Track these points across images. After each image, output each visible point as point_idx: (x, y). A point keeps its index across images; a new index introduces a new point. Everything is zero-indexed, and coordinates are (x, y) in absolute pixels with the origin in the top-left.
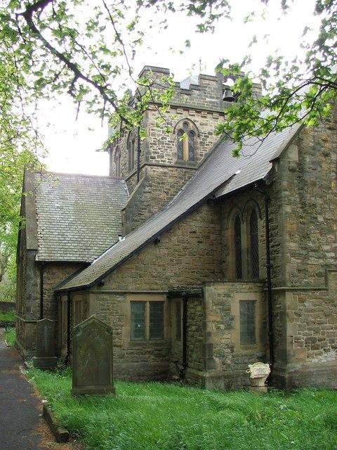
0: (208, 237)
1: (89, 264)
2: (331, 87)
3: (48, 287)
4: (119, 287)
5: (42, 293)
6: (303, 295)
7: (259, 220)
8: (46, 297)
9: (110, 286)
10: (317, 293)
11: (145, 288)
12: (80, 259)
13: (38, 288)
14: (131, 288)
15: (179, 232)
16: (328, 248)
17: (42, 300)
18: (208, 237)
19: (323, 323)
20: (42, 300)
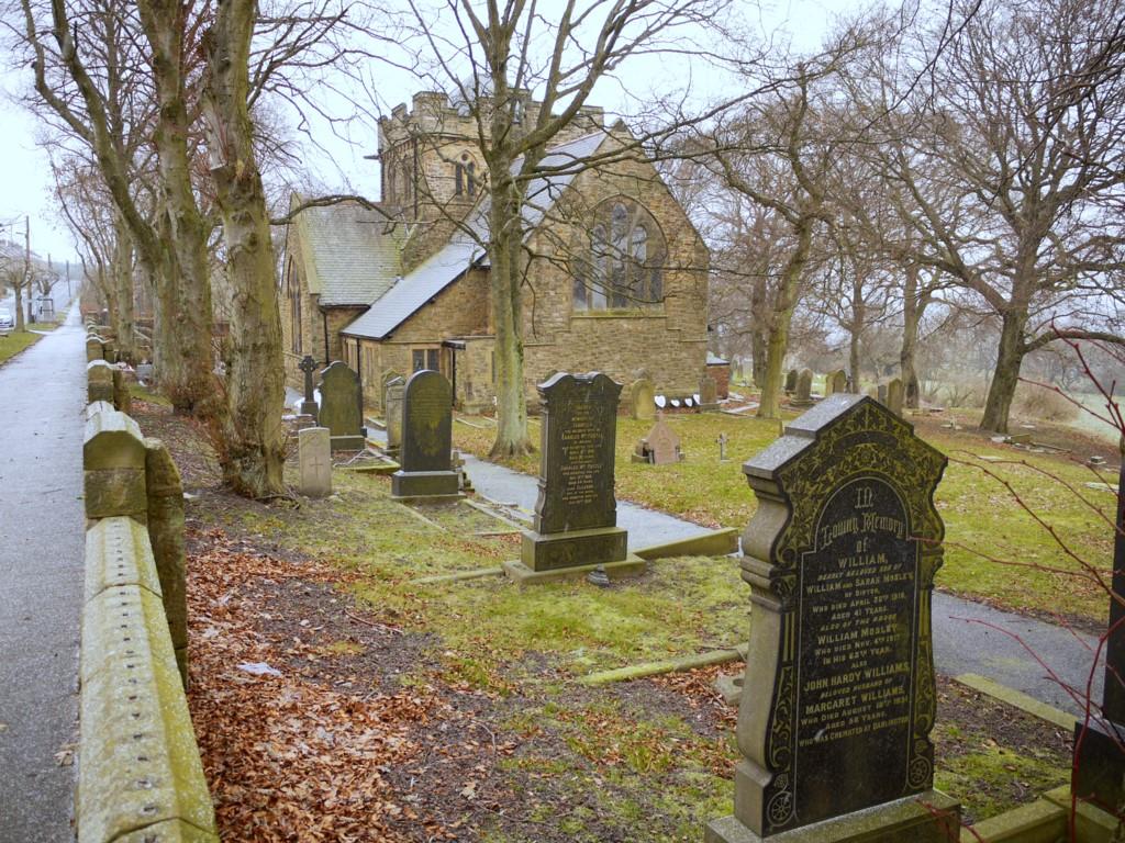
0: (475, 297)
1: (369, 307)
2: (459, 180)
3: (333, 329)
4: (403, 339)
5: (326, 335)
6: (535, 349)
7: (1073, 424)
8: (330, 338)
9: (398, 338)
10: (547, 348)
11: (424, 339)
12: (362, 302)
13: (323, 330)
14: (414, 339)
15: (451, 294)
16: (557, 314)
17: (326, 340)
18: (475, 297)
19: (146, 826)
20: (326, 340)
